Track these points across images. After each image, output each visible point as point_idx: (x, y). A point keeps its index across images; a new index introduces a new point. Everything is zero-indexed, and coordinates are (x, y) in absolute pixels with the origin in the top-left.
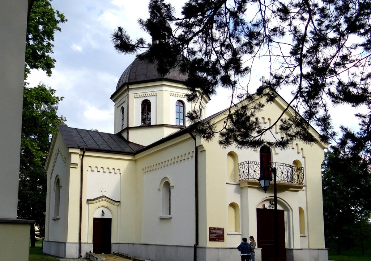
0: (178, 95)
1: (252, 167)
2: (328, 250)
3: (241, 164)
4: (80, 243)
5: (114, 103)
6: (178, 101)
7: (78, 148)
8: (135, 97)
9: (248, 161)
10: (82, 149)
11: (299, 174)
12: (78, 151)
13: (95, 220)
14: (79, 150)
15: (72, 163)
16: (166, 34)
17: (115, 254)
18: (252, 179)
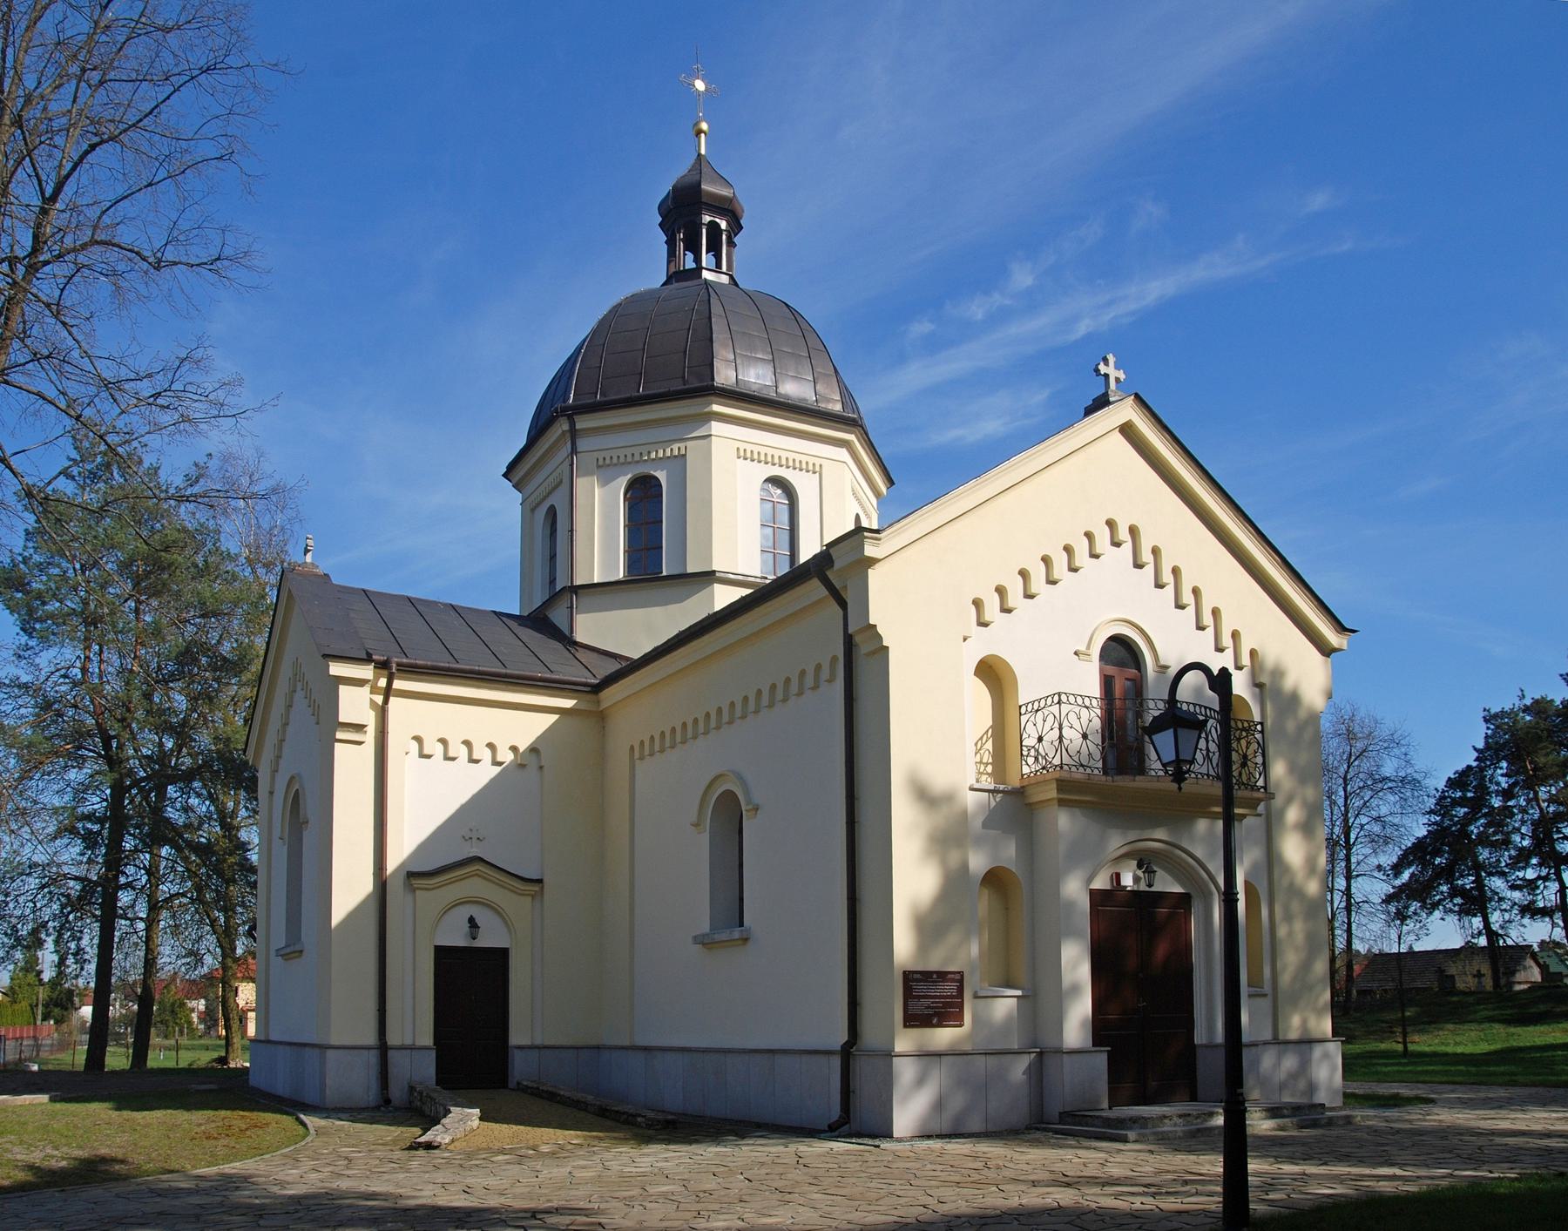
1: (1072, 717)
2: (1342, 1041)
3: (1030, 706)
4: (383, 1048)
5: (518, 496)
6: (766, 481)
7: (367, 659)
8: (601, 462)
9: (1059, 694)
10: (383, 666)
11: (1247, 748)
12: (366, 672)
13: (441, 953)
14: (372, 667)
15: (340, 720)
16: (718, 225)
17: (521, 1088)
18: (1074, 769)
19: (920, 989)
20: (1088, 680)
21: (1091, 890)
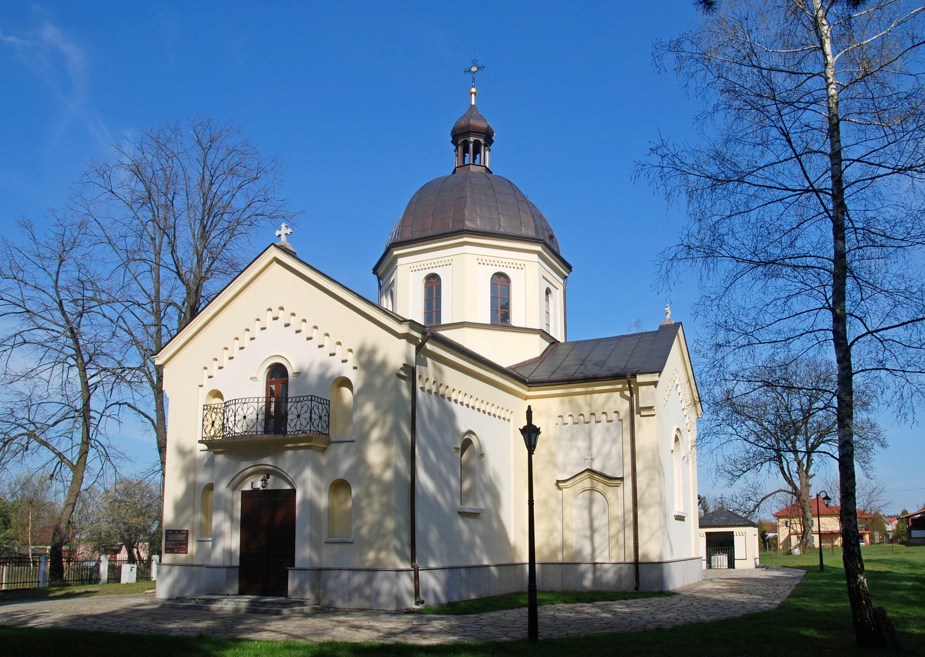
0: (492, 261)
3: (240, 401)
9: (312, 396)
19: (171, 537)
20: (259, 390)
21: (242, 491)
